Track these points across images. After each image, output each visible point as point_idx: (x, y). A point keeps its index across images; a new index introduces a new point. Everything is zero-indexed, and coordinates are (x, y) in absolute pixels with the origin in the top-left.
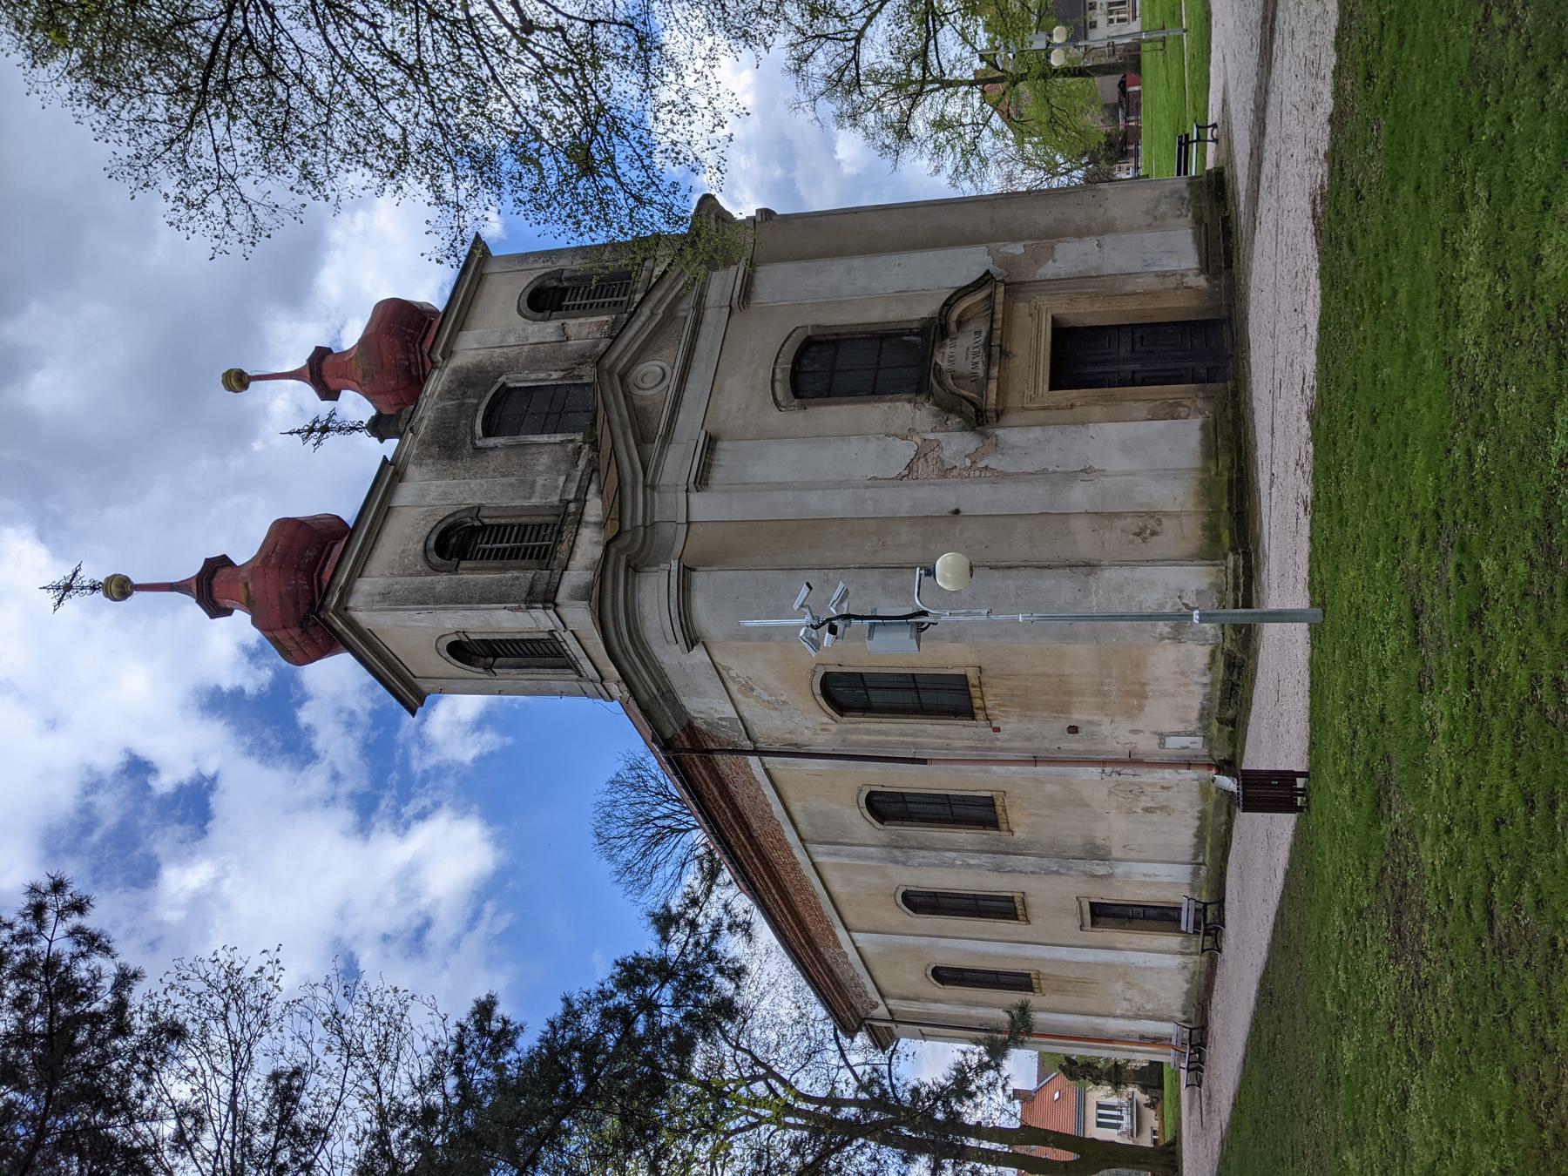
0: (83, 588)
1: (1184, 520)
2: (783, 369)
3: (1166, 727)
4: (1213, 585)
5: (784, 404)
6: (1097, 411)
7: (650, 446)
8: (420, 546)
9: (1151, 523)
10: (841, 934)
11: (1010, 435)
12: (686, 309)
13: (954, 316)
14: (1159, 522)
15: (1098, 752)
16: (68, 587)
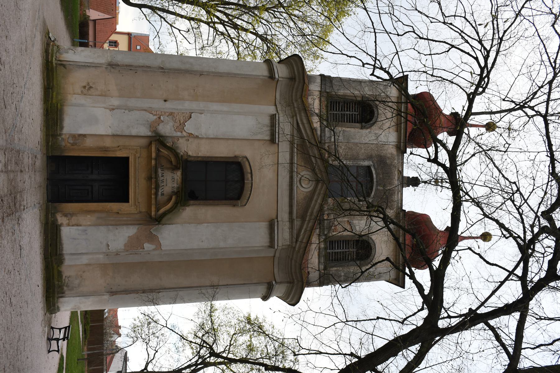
2: (248, 180)
4: (61, 54)
5: (245, 159)
6: (108, 143)
7: (298, 143)
11: (145, 131)
12: (297, 223)
14: (82, 92)
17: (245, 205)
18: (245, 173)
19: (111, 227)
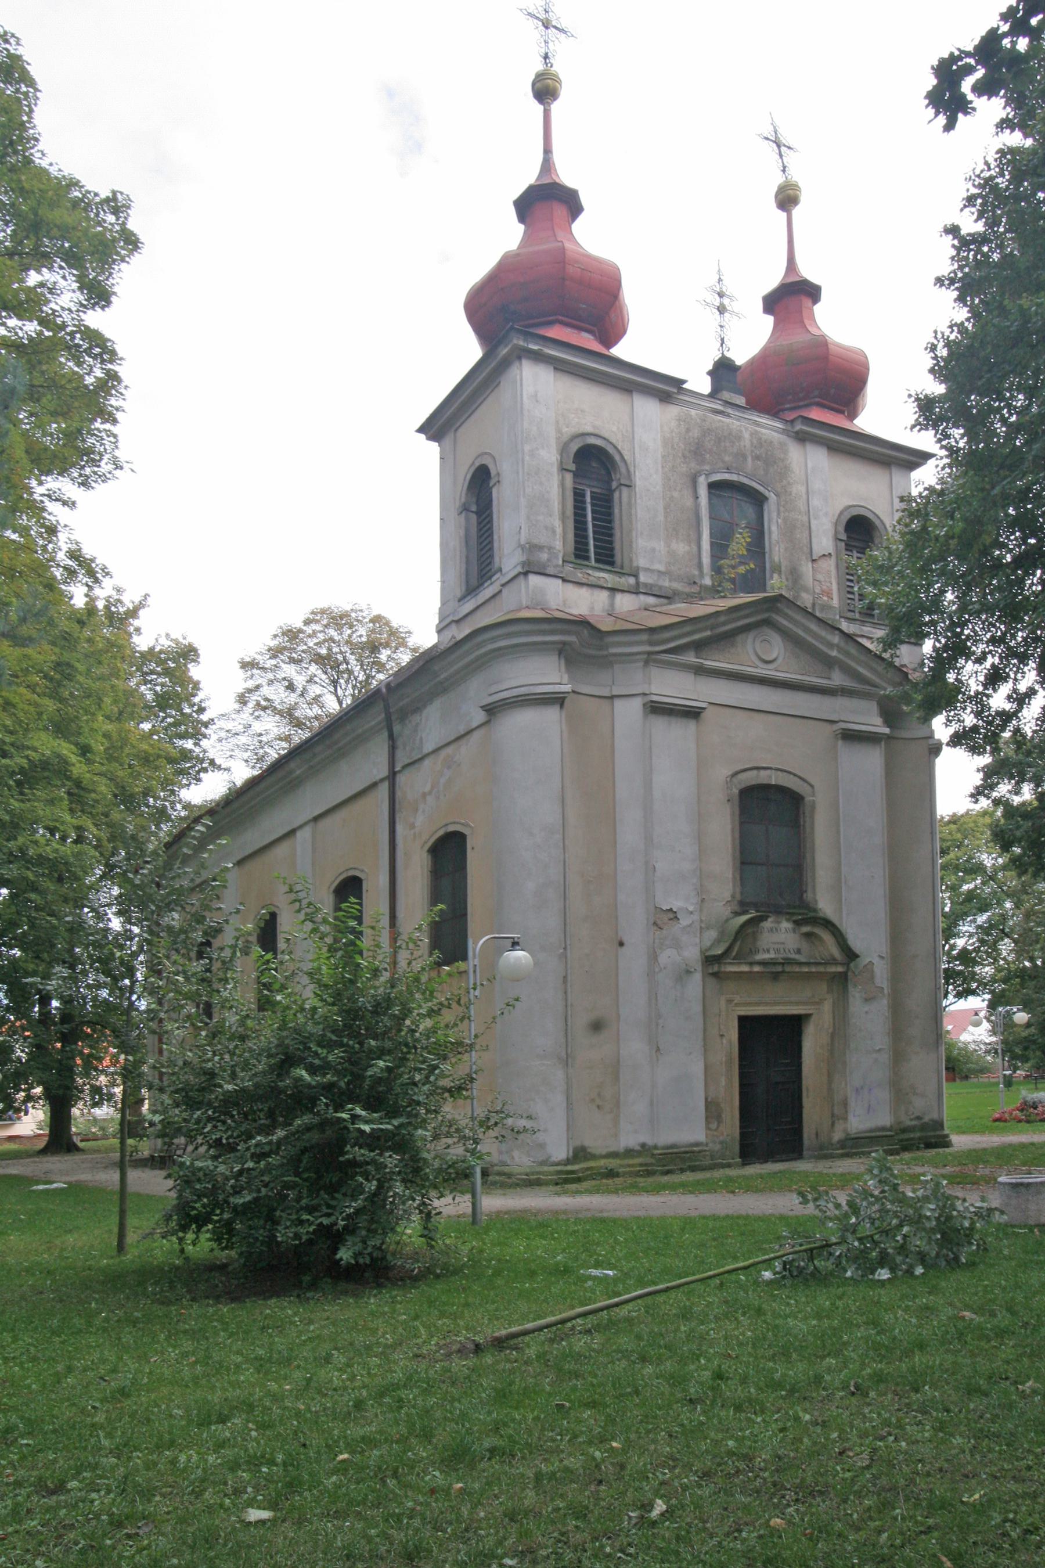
0: (546, 42)
5: (734, 780)
8: (589, 429)
13: (819, 931)
16: (547, 25)
17: (812, 786)
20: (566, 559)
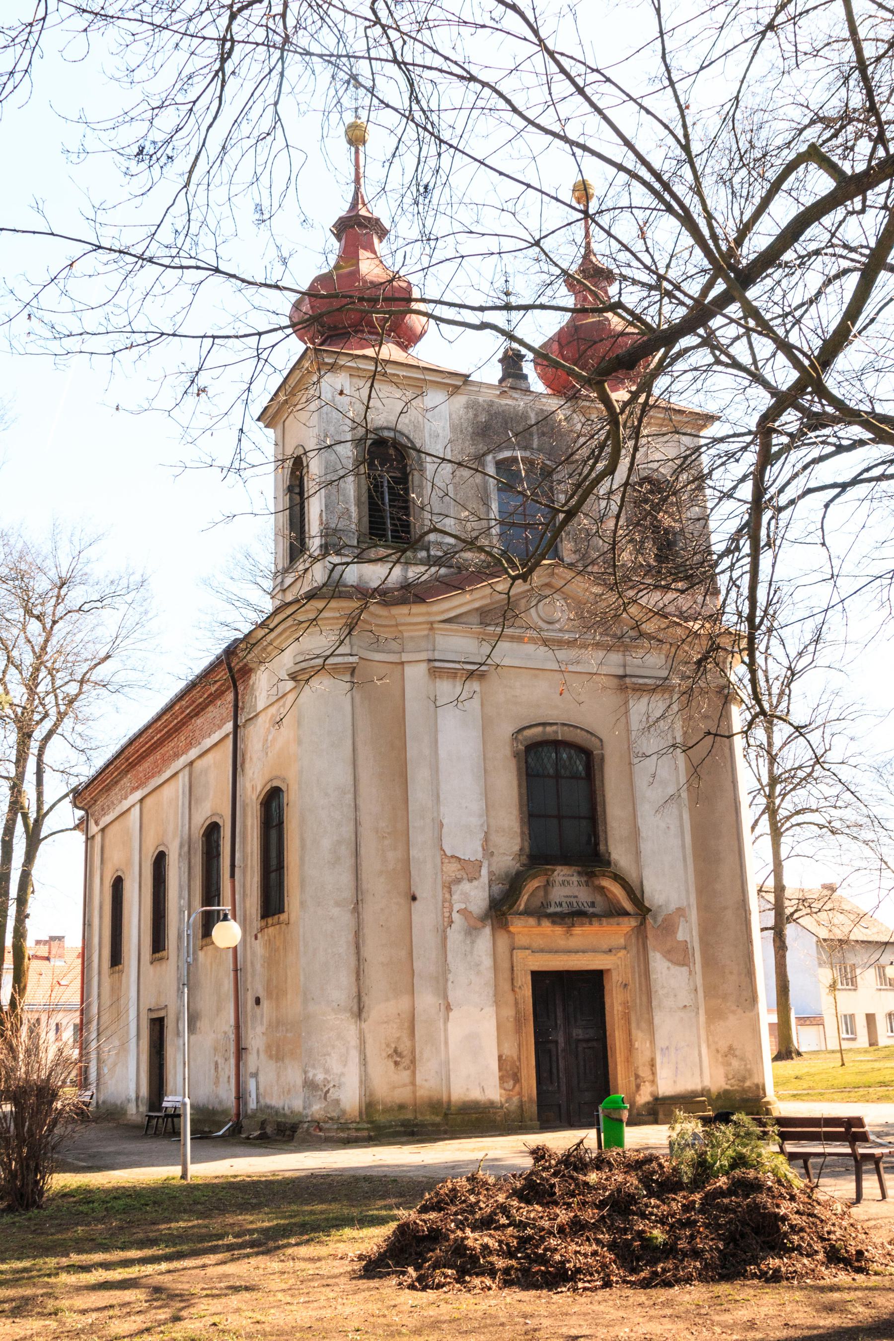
1: (409, 1088)
2: (556, 732)
3: (261, 1078)
4: (344, 1112)
5: (520, 737)
6: (509, 1012)
9: (406, 1062)
10: (138, 795)
15: (246, 1022)
17: (601, 740)
18: (545, 738)
19: (654, 1004)
20: (362, 539)
